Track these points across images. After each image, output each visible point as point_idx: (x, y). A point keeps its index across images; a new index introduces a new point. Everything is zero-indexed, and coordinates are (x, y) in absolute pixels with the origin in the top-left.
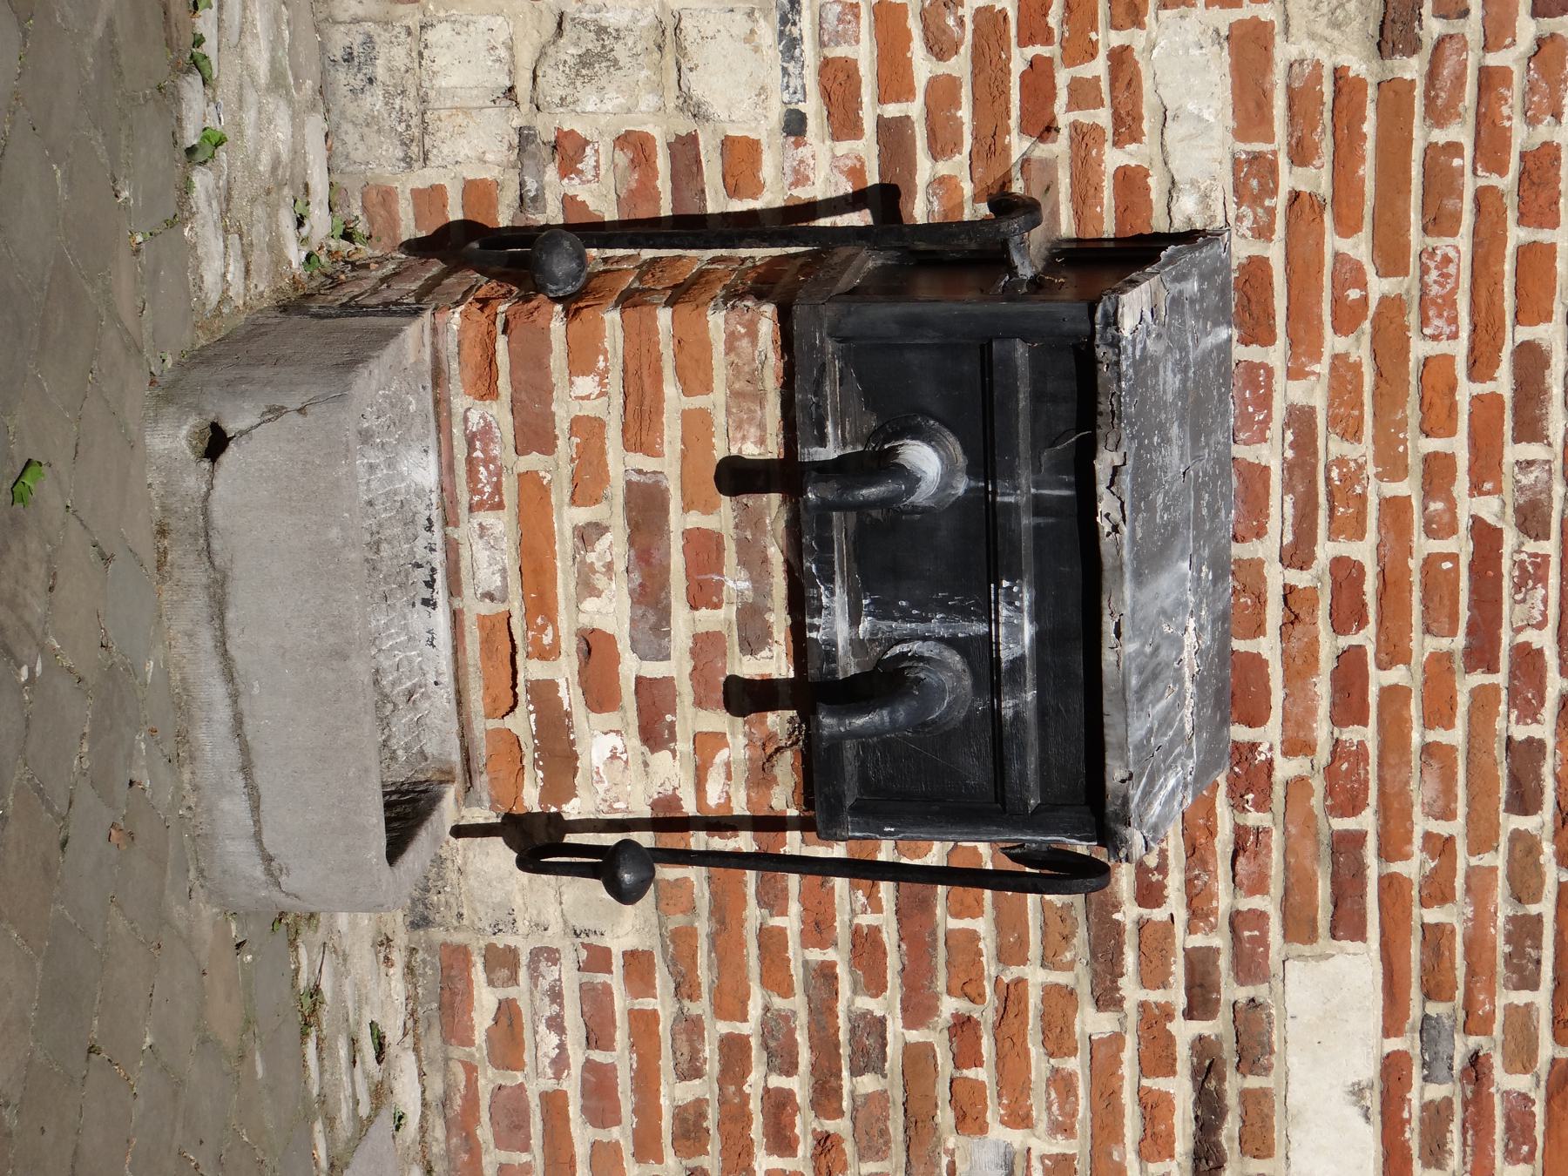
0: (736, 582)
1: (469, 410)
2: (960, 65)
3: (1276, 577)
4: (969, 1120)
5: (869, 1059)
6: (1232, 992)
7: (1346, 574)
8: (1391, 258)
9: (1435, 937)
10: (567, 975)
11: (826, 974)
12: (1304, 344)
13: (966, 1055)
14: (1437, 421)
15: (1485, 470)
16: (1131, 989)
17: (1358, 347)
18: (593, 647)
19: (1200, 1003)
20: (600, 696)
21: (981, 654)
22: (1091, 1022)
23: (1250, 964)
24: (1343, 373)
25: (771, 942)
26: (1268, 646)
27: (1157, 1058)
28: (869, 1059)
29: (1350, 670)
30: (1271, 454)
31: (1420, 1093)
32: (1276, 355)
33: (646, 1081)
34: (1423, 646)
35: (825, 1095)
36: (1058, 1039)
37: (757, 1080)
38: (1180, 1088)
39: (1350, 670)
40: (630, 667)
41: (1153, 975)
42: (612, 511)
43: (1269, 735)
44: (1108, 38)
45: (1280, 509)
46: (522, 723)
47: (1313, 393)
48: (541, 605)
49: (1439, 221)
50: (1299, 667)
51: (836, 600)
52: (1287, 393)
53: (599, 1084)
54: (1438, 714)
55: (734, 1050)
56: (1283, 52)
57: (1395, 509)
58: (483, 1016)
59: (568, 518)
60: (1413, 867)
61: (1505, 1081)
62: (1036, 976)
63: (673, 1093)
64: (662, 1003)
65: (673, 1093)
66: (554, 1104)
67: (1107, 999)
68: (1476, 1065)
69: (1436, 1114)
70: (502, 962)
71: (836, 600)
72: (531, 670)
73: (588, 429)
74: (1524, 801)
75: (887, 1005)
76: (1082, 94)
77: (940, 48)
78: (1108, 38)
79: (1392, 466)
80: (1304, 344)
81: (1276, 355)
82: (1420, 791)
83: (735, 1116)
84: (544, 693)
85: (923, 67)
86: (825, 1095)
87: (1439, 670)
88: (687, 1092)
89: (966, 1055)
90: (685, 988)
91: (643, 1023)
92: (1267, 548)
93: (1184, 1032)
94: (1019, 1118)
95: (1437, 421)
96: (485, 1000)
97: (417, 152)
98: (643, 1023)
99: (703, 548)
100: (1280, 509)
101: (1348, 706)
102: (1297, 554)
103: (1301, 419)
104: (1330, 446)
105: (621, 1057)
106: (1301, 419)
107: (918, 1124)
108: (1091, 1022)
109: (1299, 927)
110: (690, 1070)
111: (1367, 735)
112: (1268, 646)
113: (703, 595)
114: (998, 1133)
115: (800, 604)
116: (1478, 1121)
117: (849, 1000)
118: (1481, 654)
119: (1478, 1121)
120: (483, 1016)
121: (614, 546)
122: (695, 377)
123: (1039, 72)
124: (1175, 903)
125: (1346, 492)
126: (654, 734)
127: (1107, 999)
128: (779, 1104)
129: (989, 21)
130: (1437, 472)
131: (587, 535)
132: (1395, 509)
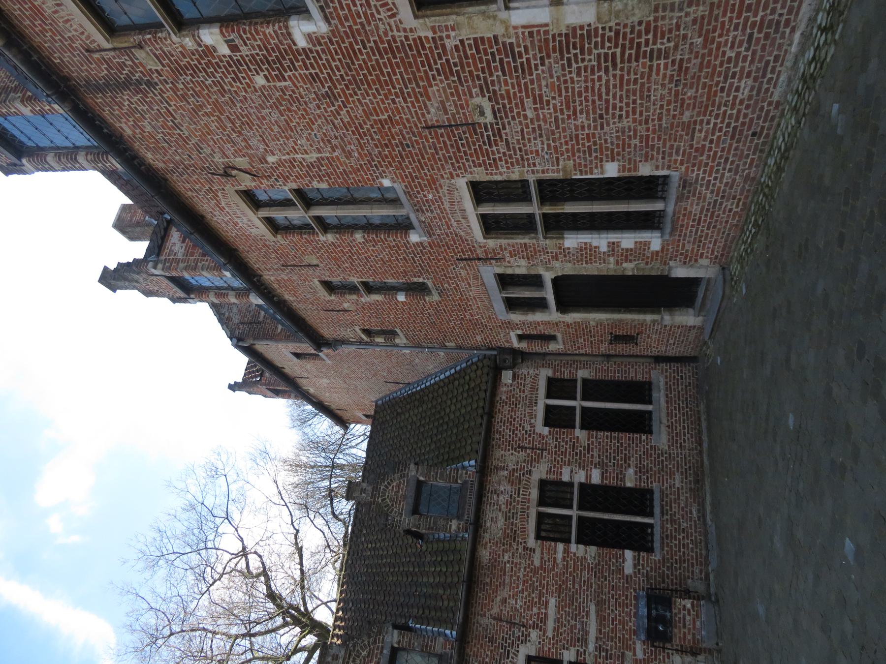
0: (677, 619)
1: (699, 637)
2: (658, 657)
3: (633, 608)
4: (659, 560)
5: (668, 567)
6: (636, 570)
7: (627, 608)
8: (623, 635)
9: (620, 574)
10: (696, 578)
11: (672, 575)
12: (630, 628)
13: (660, 567)
14: (620, 620)
15: (616, 615)
16: (645, 572)
17: (626, 627)
18: (689, 614)
19: (639, 570)
20: (689, 611)
21: (657, 610)
22: (648, 569)
23: (635, 573)
24: (627, 626)
25: (676, 579)
26: (633, 602)
27: (643, 565)
28: (668, 567)
29: (627, 599)
30: (633, 619)
31: (621, 560)
32: (633, 628)
33: (688, 566)
34: (621, 600)
35: (672, 564)
36: (651, 568)
37: (678, 566)
38: (641, 562)
39: (627, 599)
40: (686, 612)
41: (643, 573)
42: (687, 626)
43: (633, 594)
44: (646, 657)
45: (632, 614)
46: (696, 609)
47: (630, 624)
48: (694, 620)
49: (620, 637)
50: (631, 600)
51: (669, 617)
52: (632, 624)
53: (693, 567)
54: (620, 594)
55: (680, 569)
56: (631, 654)
57: (623, 613)
58: (703, 574)
59: (691, 626)
60: (622, 581)
61: (614, 561)
62: (653, 574)
63: (686, 565)
64: (687, 574)
65: (686, 565)
66: (697, 565)
67: (647, 571)
68: (617, 562)
69: (620, 558)
70: (701, 579)
71: (669, 617)
72: (695, 613)
73: (689, 634)
74: (613, 586)
75: (666, 572)
76: (583, 139)
77: (660, 659)
78: (646, 657)
79: (623, 617)
80: (630, 628)
81: (633, 628)
82: (621, 588)
83: (680, 563)
84: (694, 611)
85: (661, 657)
86: (672, 564)
87: (620, 598)
88: (684, 565)
89: (660, 567)
90: (684, 575)
91: (688, 572)
92: (633, 611)
93: (641, 567)
94: (655, 560)
95: (620, 620)
96: (703, 576)
97: (706, 658)
98: (688, 572)
99: (680, 622)
100: (632, 614)
101: (627, 596)
102: (631, 610)
103: (631, 622)
104: (628, 619)
105: (691, 569)
106: (631, 622)
107: (664, 560)
108: (648, 569)
109: (631, 576)
110: (684, 567)
111: (625, 593)
112: (633, 602)
113: (680, 618)
114: (657, 559)
115: (671, 617)
116: (617, 557)
117: (670, 573)
118: (616, 599)
119: (617, 557)
120: (703, 574)
121: (687, 623)
122: (680, 638)
123: (652, 655)
124: (641, 579)
125: (627, 615)
126: (684, 606)
127: (647, 571)
128: (676, 564)
129: (712, 4)
130: (620, 616)
131: (689, 625)
132: (623, 613)
